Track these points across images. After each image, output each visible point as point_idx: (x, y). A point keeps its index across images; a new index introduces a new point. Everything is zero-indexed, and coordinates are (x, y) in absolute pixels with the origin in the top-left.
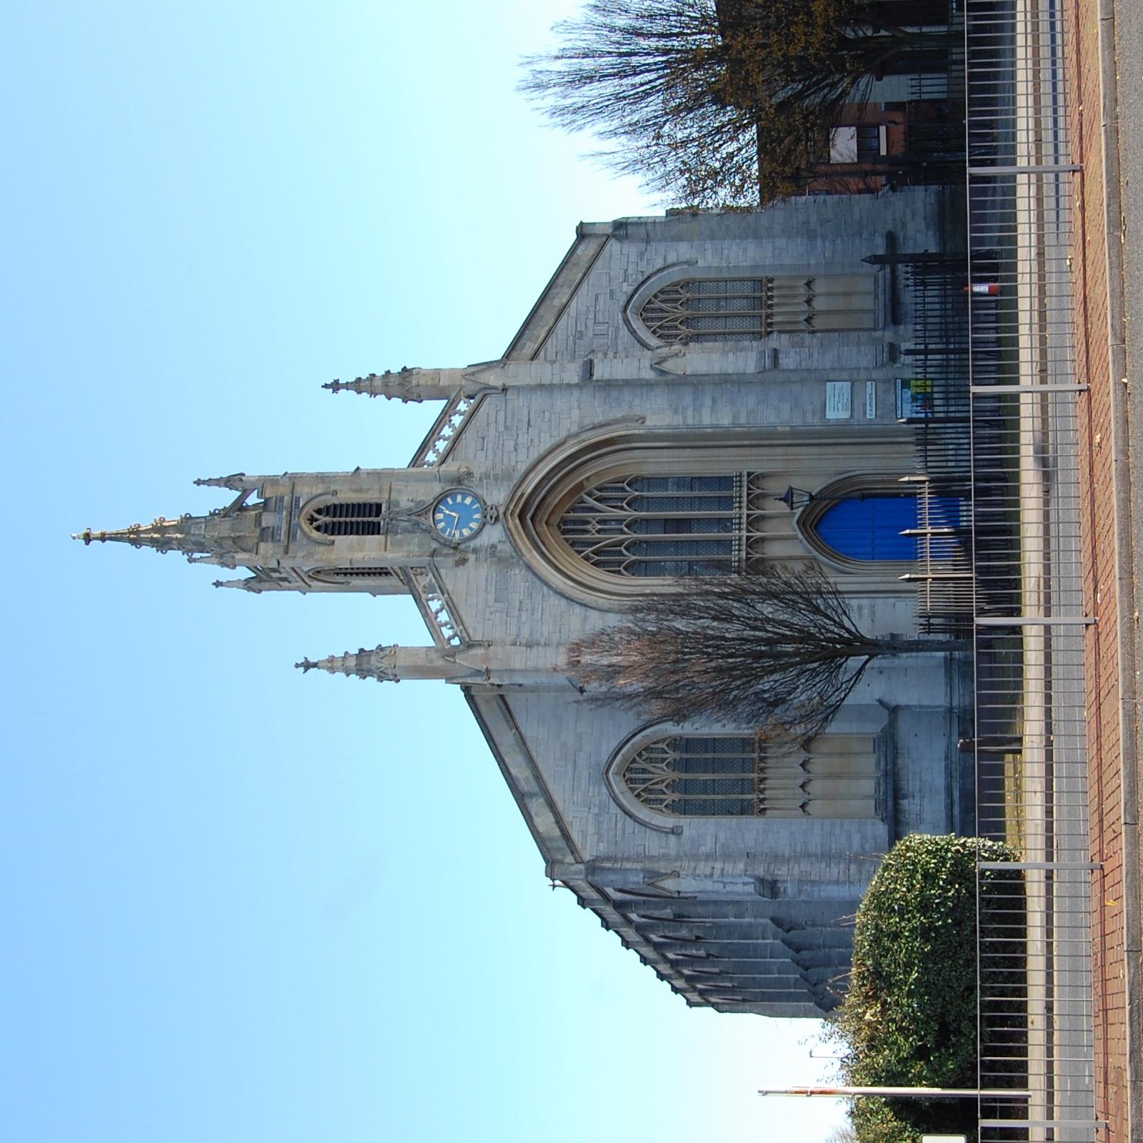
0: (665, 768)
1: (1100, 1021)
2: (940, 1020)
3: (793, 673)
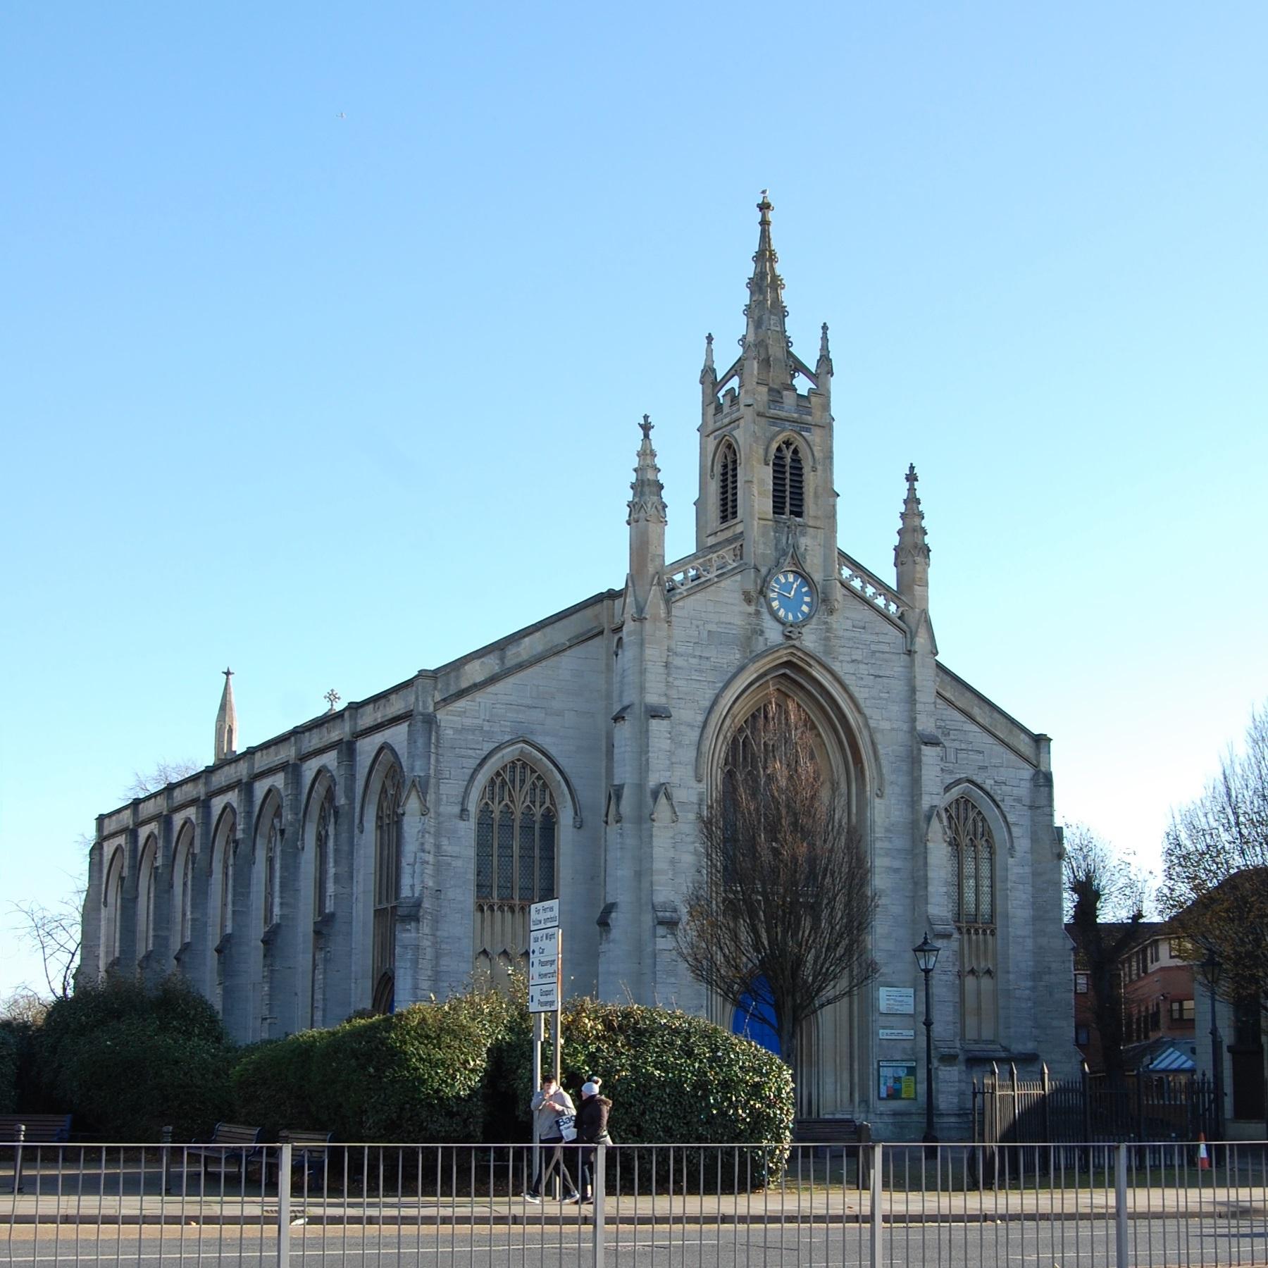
0: (525, 804)
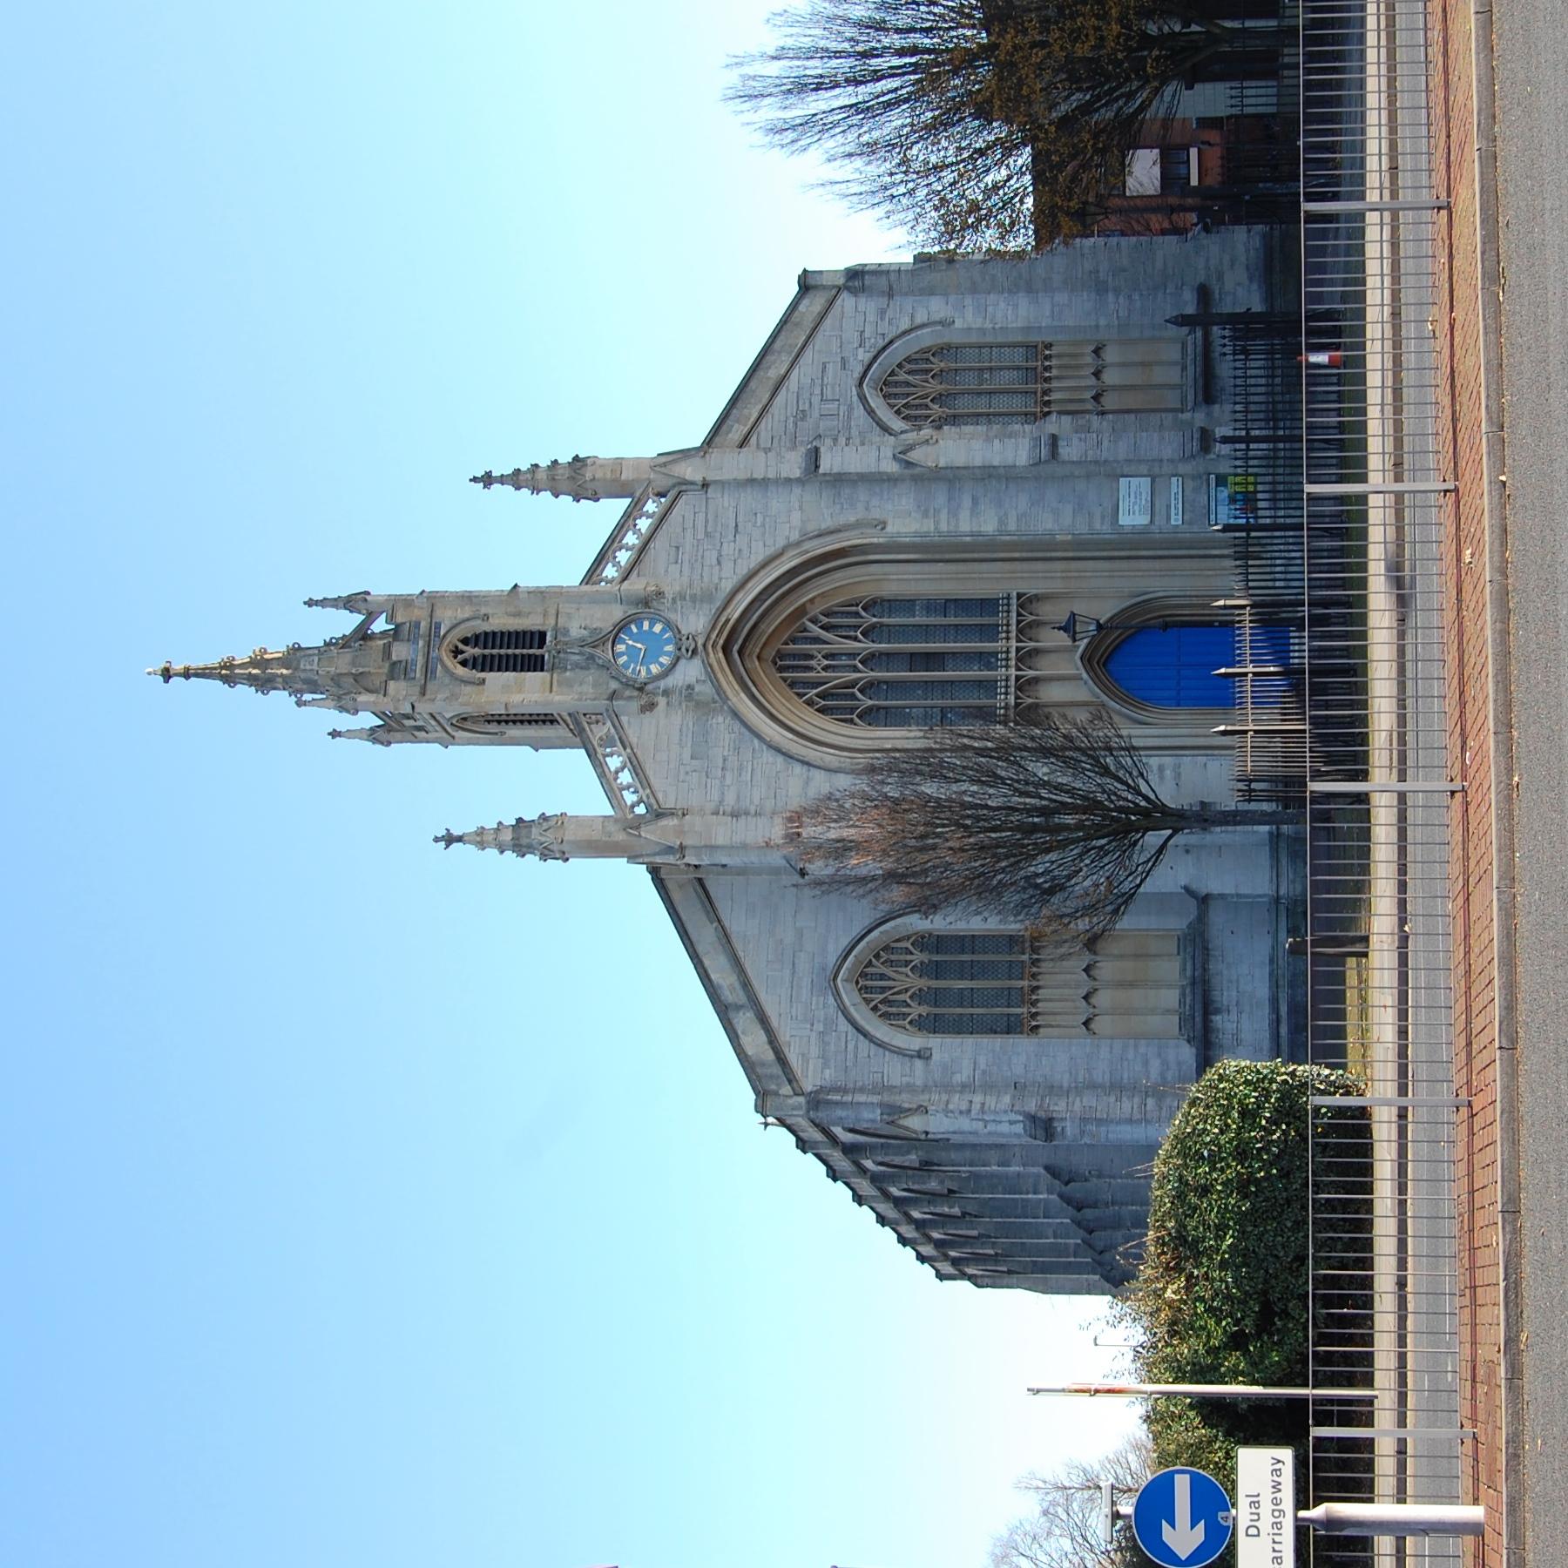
0: (910, 973)
2: (1263, 1299)
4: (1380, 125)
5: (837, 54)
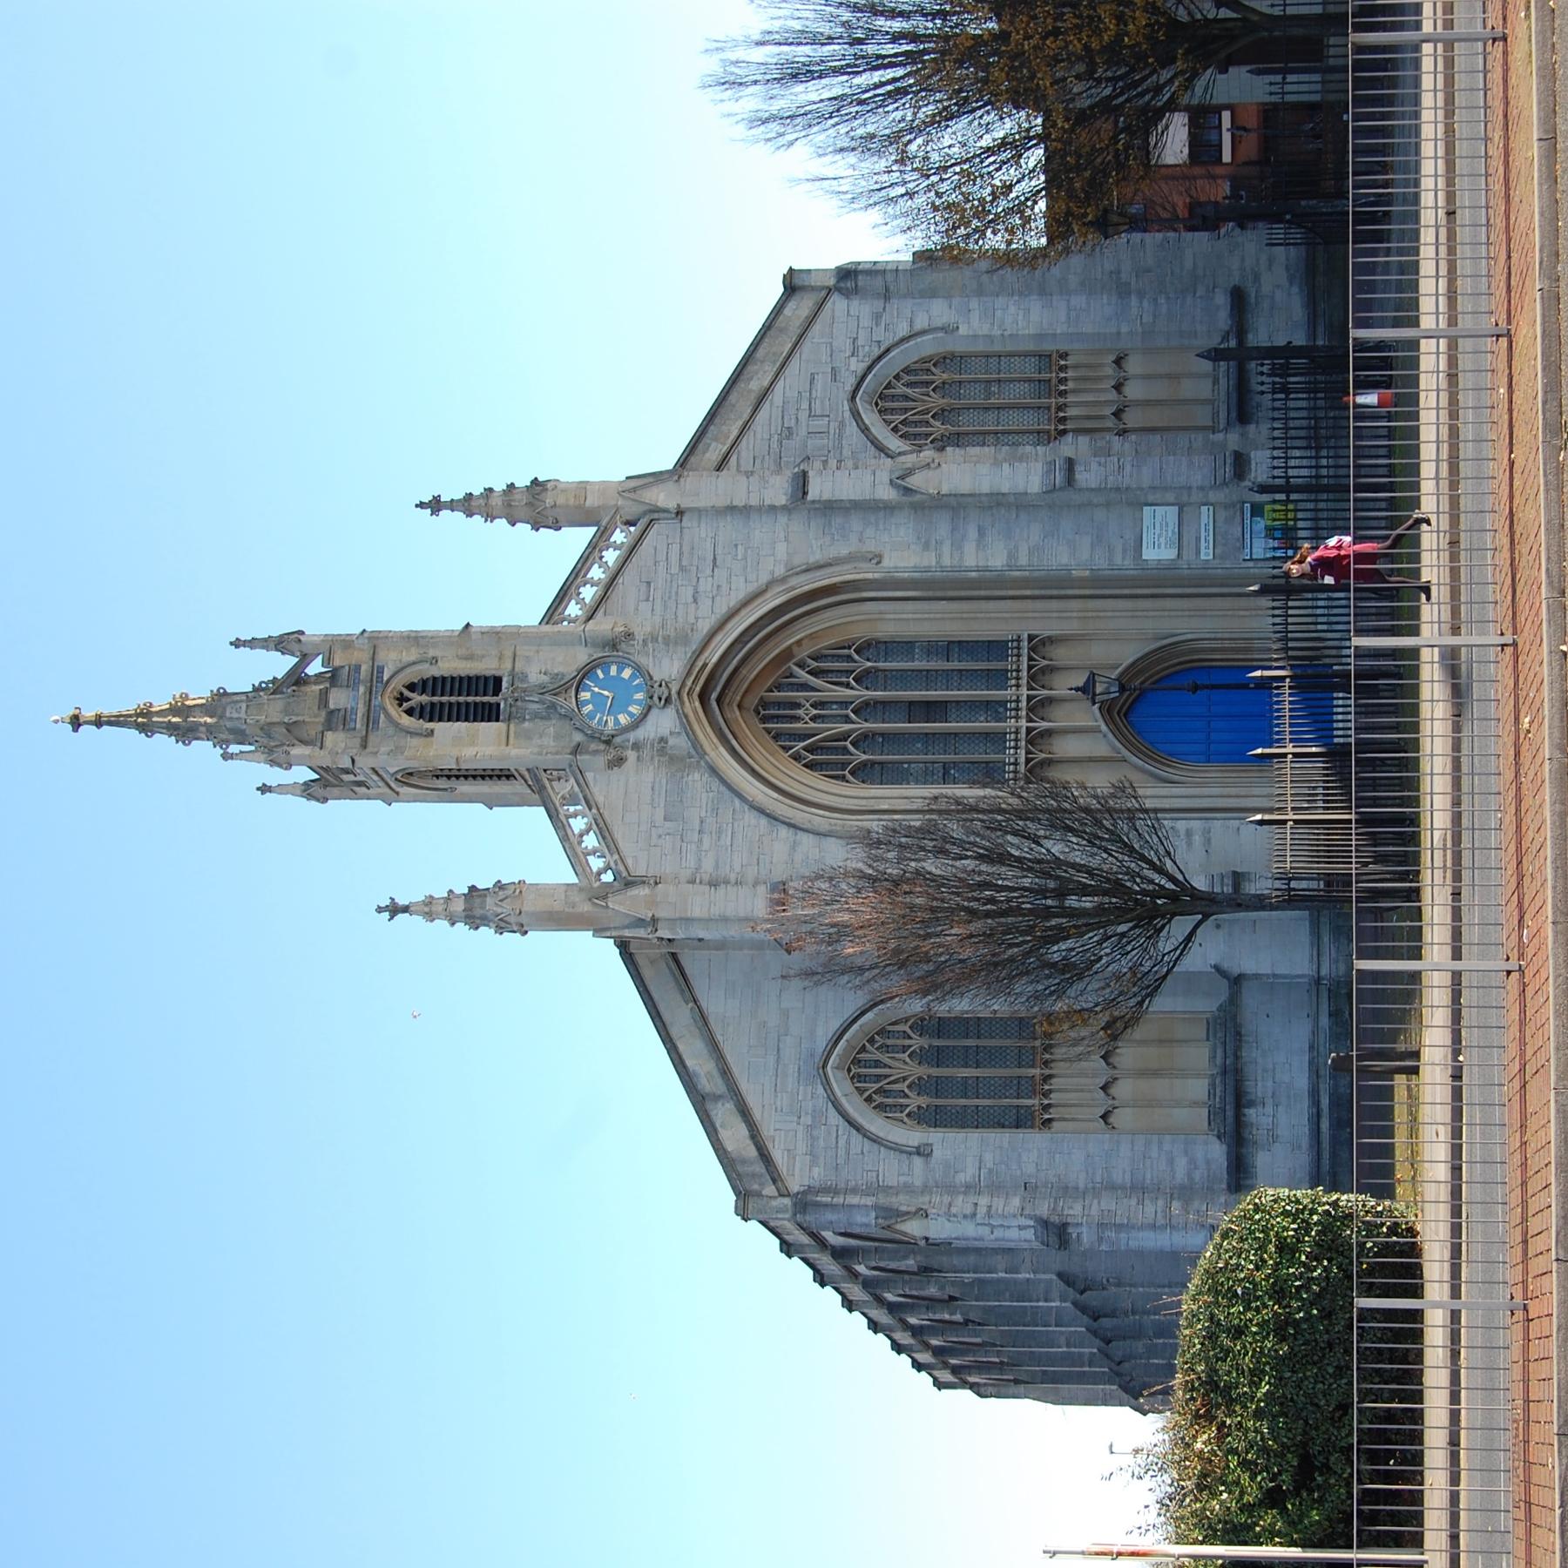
0: (908, 1060)
1: (1521, 1514)
2: (1301, 1451)
3: (1095, 939)
4: (1436, 176)
5: (830, 40)
